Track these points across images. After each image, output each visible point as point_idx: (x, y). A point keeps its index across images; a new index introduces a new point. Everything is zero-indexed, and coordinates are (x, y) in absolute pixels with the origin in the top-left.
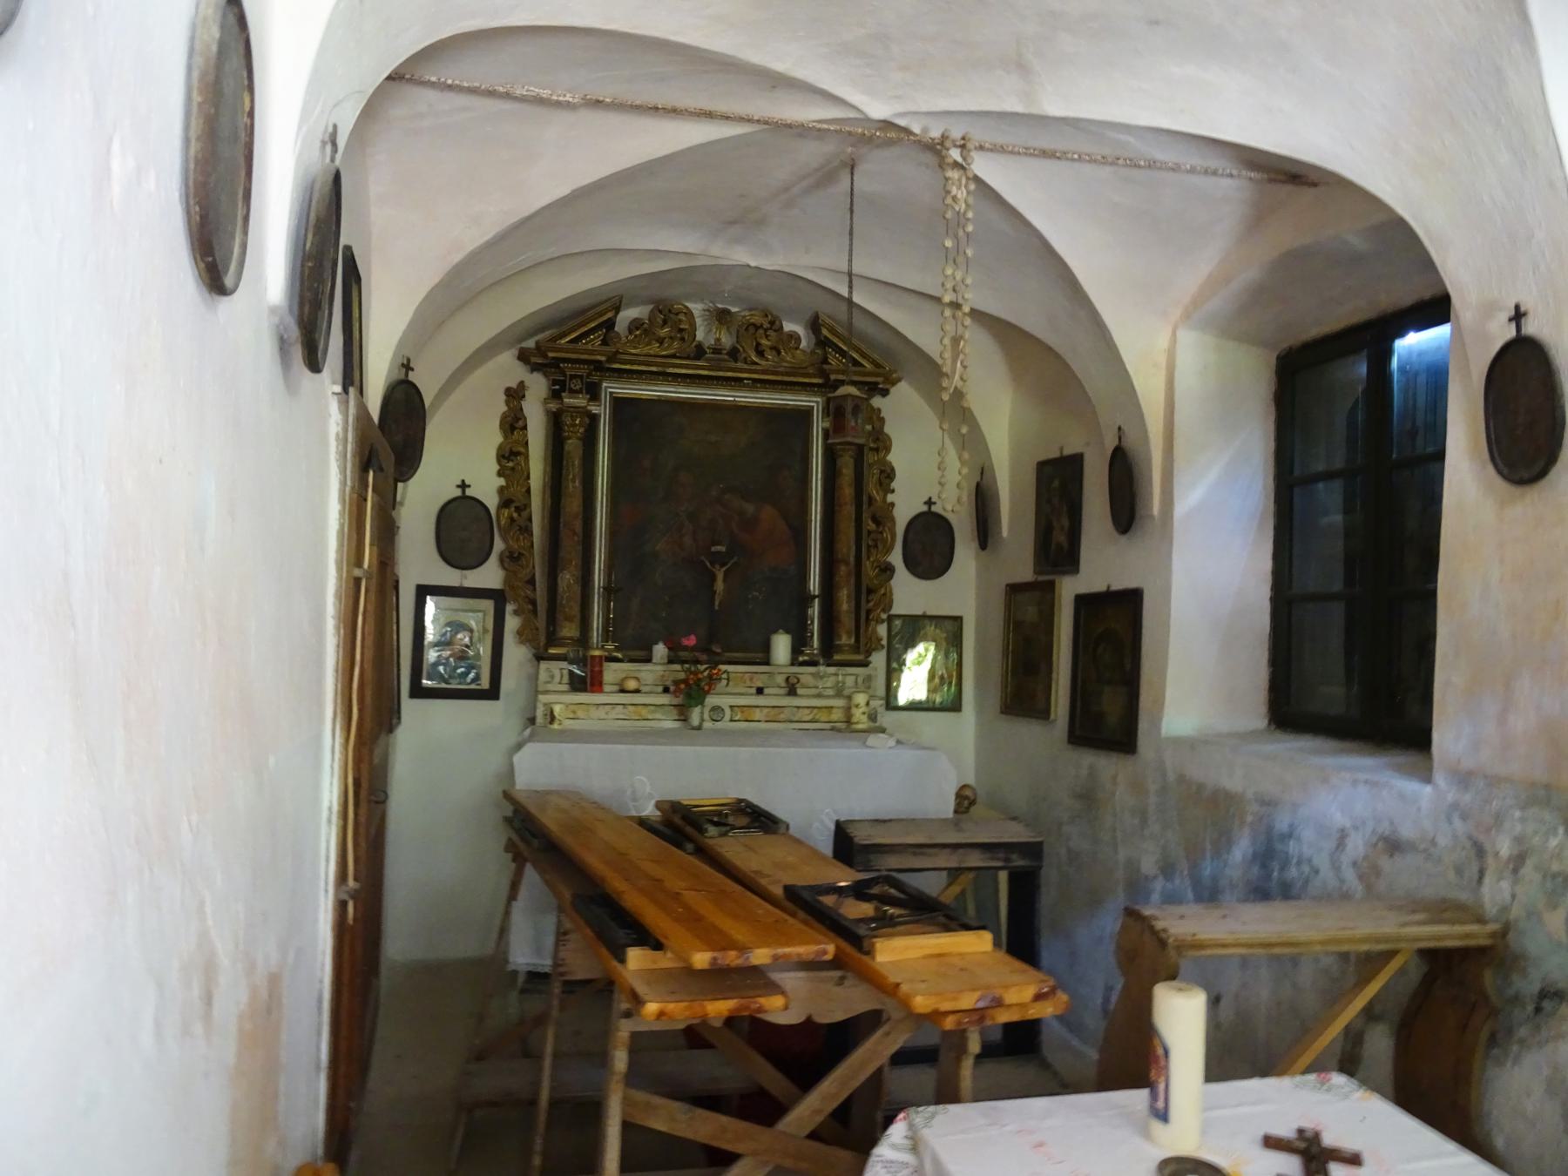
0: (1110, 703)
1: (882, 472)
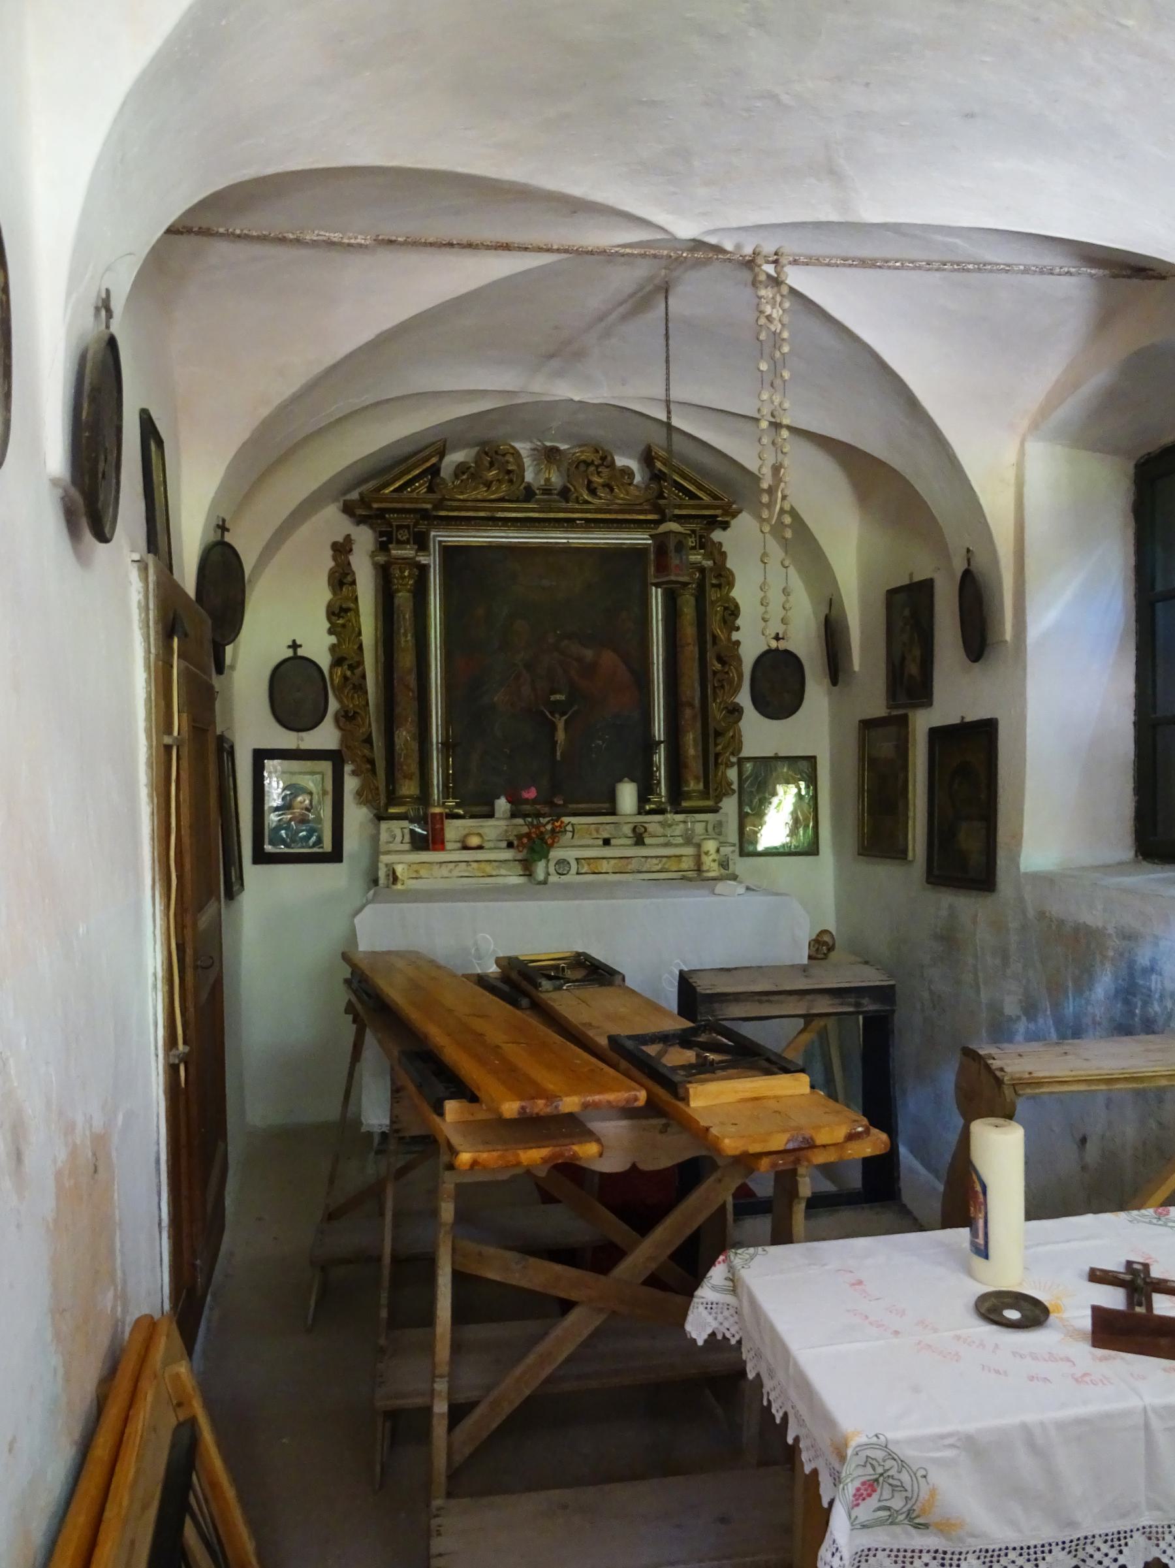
0: (968, 840)
1: (726, 609)
